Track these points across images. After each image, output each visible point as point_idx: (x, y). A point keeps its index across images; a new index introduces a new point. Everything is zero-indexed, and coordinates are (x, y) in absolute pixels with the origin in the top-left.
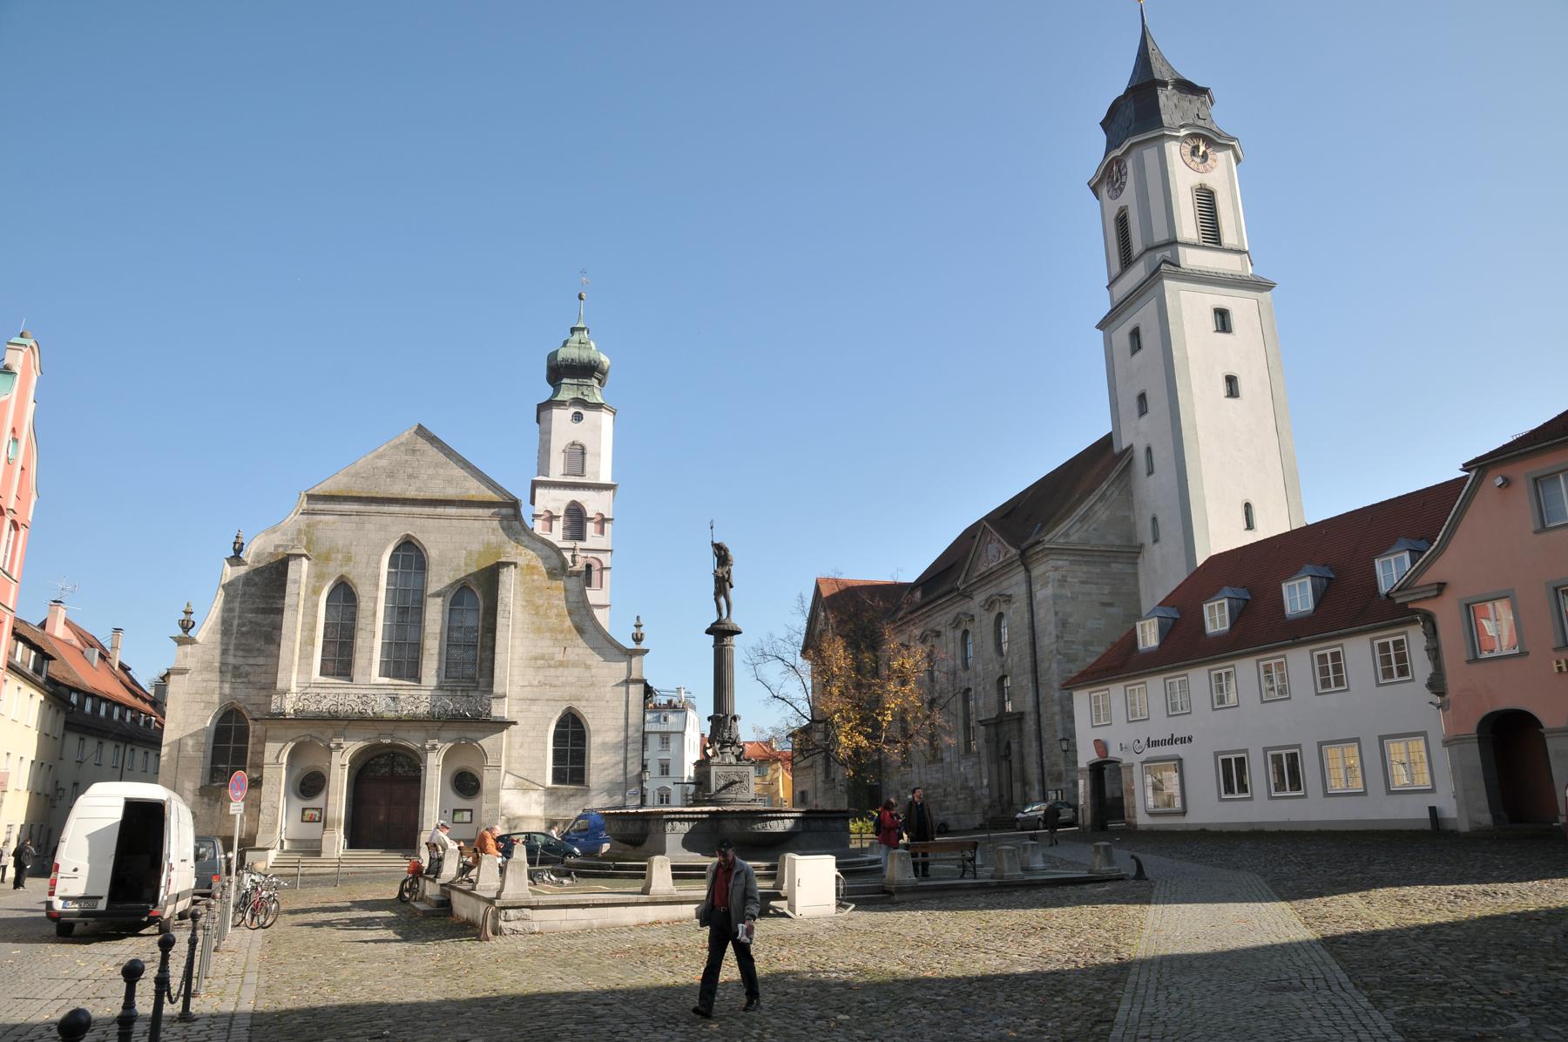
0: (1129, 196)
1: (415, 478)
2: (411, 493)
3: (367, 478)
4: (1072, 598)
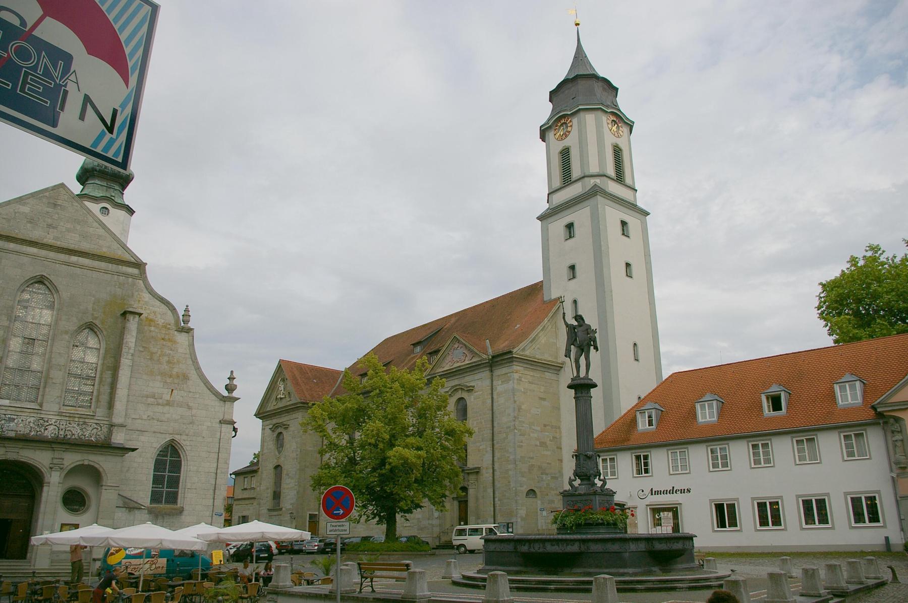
0: (571, 141)
1: (54, 228)
2: (49, 240)
3: (8, 220)
4: (524, 393)
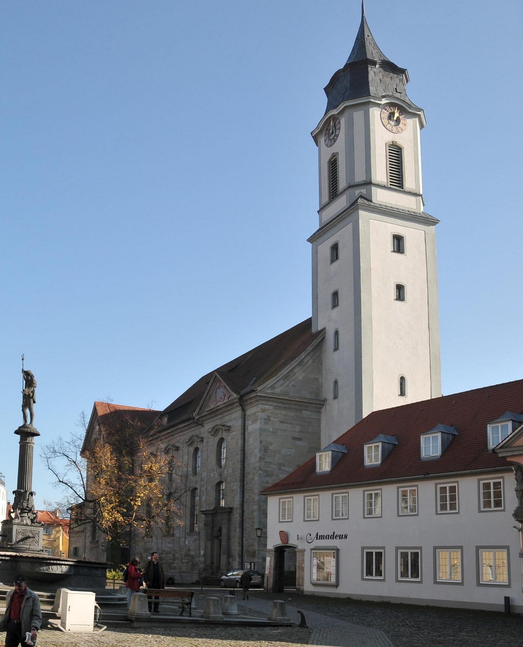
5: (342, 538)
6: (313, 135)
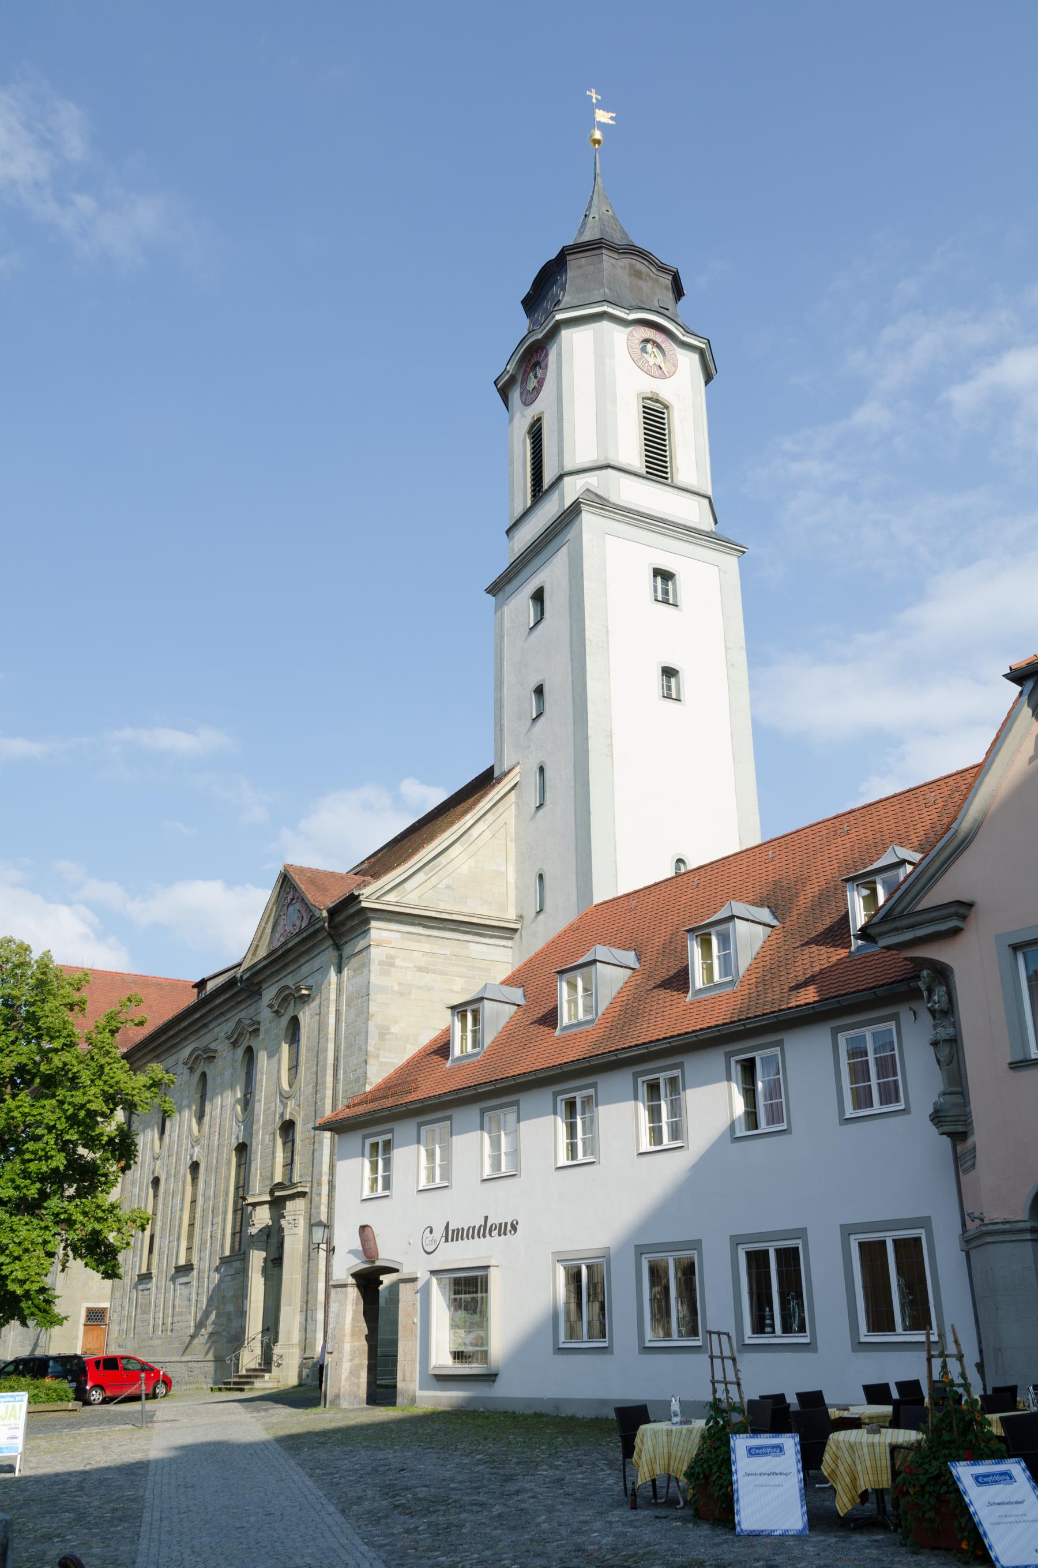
0: (543, 404)
5: (505, 1234)
6: (499, 386)
